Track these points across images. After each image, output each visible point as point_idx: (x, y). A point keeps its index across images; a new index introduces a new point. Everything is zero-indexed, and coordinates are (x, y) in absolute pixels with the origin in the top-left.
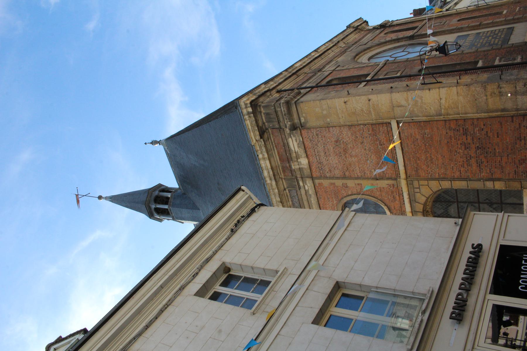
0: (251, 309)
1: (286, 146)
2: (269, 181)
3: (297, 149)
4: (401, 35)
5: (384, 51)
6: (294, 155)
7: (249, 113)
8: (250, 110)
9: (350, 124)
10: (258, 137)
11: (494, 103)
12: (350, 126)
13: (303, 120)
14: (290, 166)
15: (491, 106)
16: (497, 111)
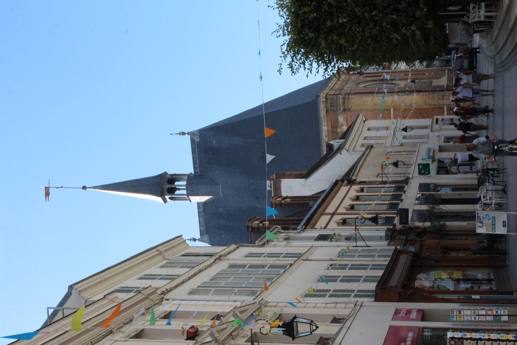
0: (445, 75)
1: (337, 120)
2: (324, 138)
3: (342, 121)
4: (369, 79)
5: (369, 85)
6: (340, 124)
7: (323, 101)
8: (324, 100)
9: (371, 109)
10: (325, 114)
11: (431, 102)
12: (372, 111)
13: (350, 106)
14: (337, 130)
15: (430, 104)
16: (432, 105)
